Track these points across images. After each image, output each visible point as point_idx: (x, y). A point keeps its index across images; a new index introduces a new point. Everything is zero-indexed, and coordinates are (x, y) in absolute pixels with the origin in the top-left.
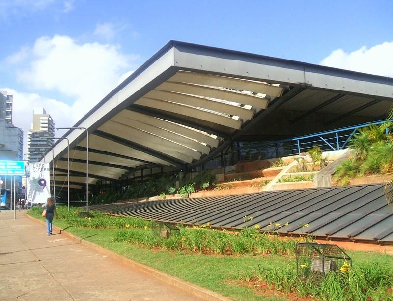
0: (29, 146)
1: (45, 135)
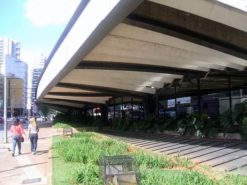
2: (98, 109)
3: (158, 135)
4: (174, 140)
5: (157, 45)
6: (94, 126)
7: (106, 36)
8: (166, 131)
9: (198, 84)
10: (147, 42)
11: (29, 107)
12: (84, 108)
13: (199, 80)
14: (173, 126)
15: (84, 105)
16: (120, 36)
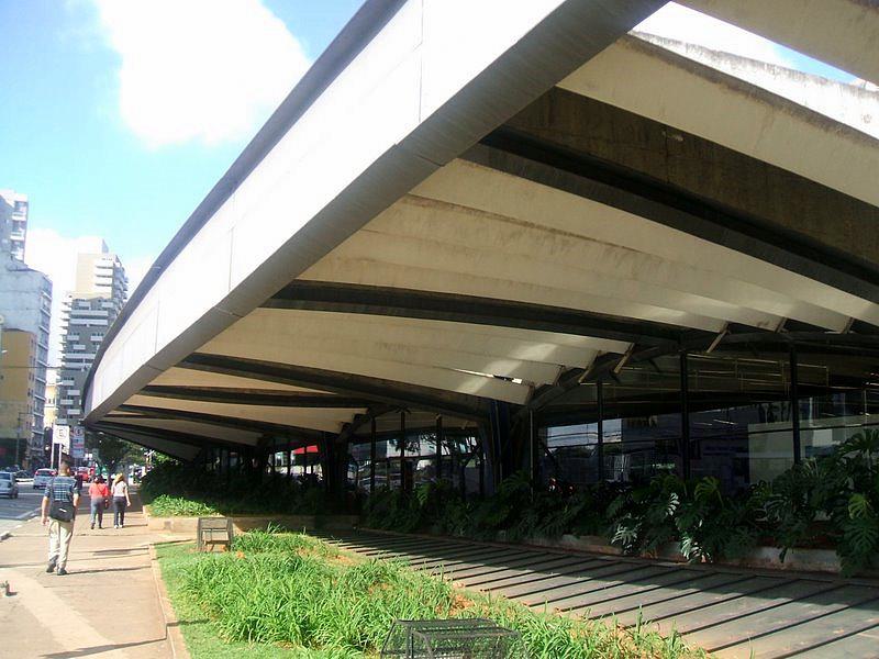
0: (65, 332)
1: (104, 305)
2: (313, 449)
3: (543, 551)
4: (607, 568)
5: (558, 237)
6: (297, 514)
7: (399, 198)
8: (569, 536)
9: (682, 374)
10: (525, 224)
11: (62, 437)
12: (240, 446)
13: (686, 361)
14: (592, 520)
15: (260, 435)
16: (434, 200)
